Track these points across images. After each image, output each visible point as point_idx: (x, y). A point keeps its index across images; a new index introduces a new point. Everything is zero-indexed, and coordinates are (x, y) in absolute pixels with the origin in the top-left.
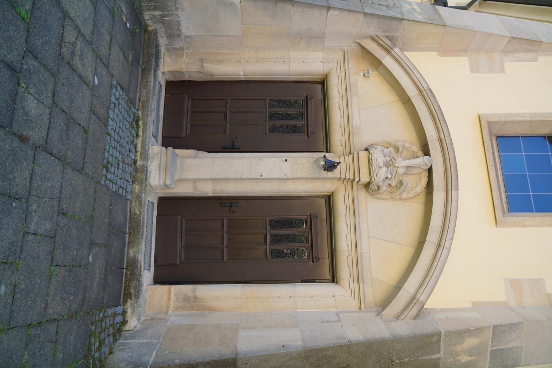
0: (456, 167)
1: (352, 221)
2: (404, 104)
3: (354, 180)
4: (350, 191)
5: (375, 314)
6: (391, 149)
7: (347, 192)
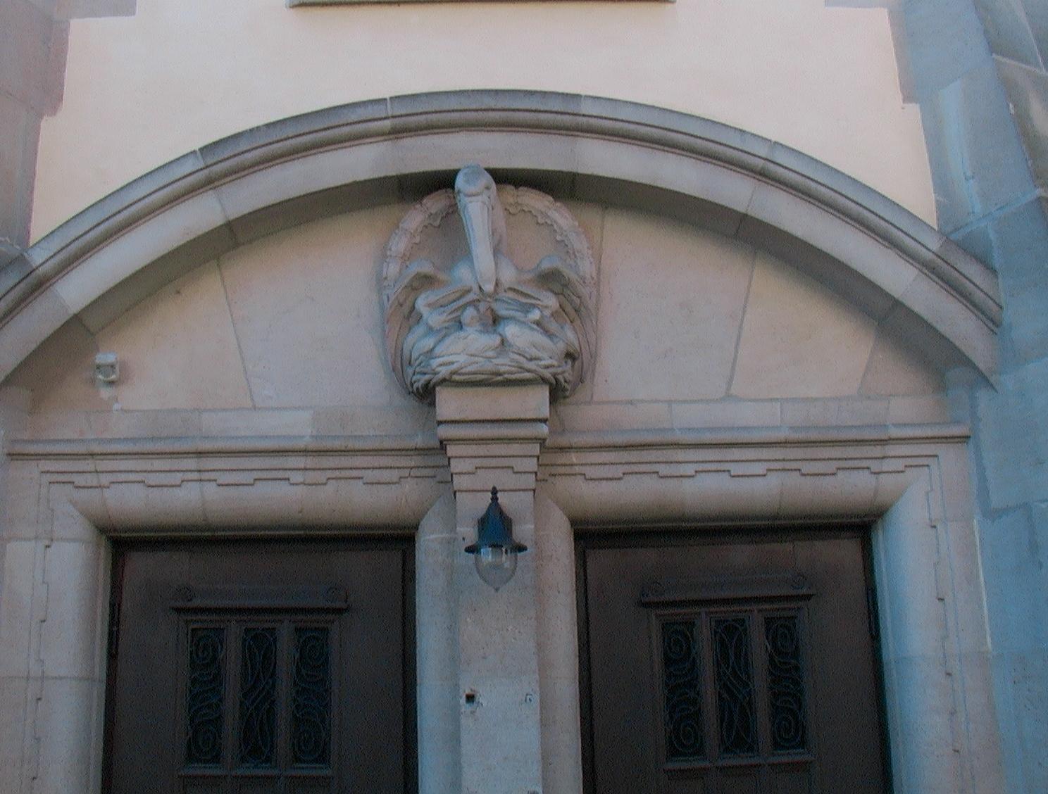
0: (497, 92)
1: (680, 455)
2: (237, 245)
3: (542, 441)
4: (574, 458)
5: (983, 396)
6: (422, 302)
7: (577, 469)
